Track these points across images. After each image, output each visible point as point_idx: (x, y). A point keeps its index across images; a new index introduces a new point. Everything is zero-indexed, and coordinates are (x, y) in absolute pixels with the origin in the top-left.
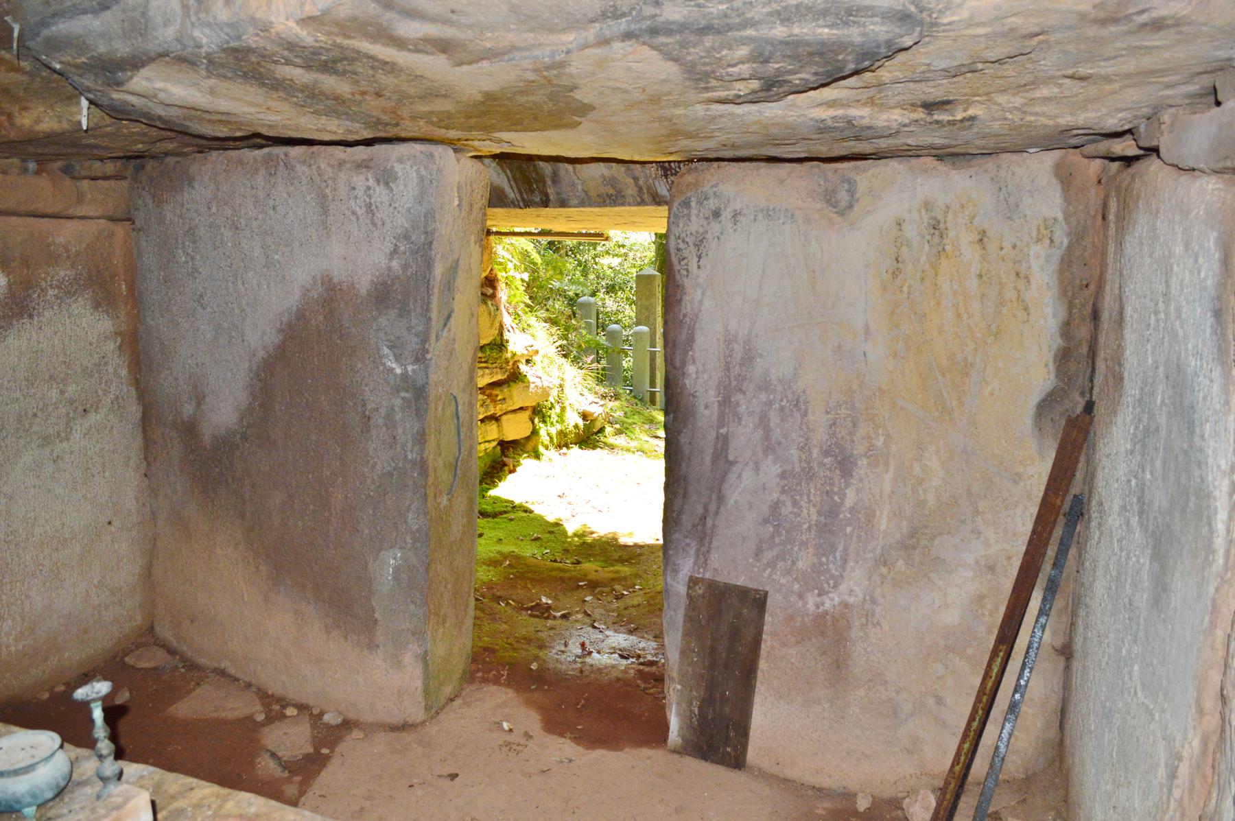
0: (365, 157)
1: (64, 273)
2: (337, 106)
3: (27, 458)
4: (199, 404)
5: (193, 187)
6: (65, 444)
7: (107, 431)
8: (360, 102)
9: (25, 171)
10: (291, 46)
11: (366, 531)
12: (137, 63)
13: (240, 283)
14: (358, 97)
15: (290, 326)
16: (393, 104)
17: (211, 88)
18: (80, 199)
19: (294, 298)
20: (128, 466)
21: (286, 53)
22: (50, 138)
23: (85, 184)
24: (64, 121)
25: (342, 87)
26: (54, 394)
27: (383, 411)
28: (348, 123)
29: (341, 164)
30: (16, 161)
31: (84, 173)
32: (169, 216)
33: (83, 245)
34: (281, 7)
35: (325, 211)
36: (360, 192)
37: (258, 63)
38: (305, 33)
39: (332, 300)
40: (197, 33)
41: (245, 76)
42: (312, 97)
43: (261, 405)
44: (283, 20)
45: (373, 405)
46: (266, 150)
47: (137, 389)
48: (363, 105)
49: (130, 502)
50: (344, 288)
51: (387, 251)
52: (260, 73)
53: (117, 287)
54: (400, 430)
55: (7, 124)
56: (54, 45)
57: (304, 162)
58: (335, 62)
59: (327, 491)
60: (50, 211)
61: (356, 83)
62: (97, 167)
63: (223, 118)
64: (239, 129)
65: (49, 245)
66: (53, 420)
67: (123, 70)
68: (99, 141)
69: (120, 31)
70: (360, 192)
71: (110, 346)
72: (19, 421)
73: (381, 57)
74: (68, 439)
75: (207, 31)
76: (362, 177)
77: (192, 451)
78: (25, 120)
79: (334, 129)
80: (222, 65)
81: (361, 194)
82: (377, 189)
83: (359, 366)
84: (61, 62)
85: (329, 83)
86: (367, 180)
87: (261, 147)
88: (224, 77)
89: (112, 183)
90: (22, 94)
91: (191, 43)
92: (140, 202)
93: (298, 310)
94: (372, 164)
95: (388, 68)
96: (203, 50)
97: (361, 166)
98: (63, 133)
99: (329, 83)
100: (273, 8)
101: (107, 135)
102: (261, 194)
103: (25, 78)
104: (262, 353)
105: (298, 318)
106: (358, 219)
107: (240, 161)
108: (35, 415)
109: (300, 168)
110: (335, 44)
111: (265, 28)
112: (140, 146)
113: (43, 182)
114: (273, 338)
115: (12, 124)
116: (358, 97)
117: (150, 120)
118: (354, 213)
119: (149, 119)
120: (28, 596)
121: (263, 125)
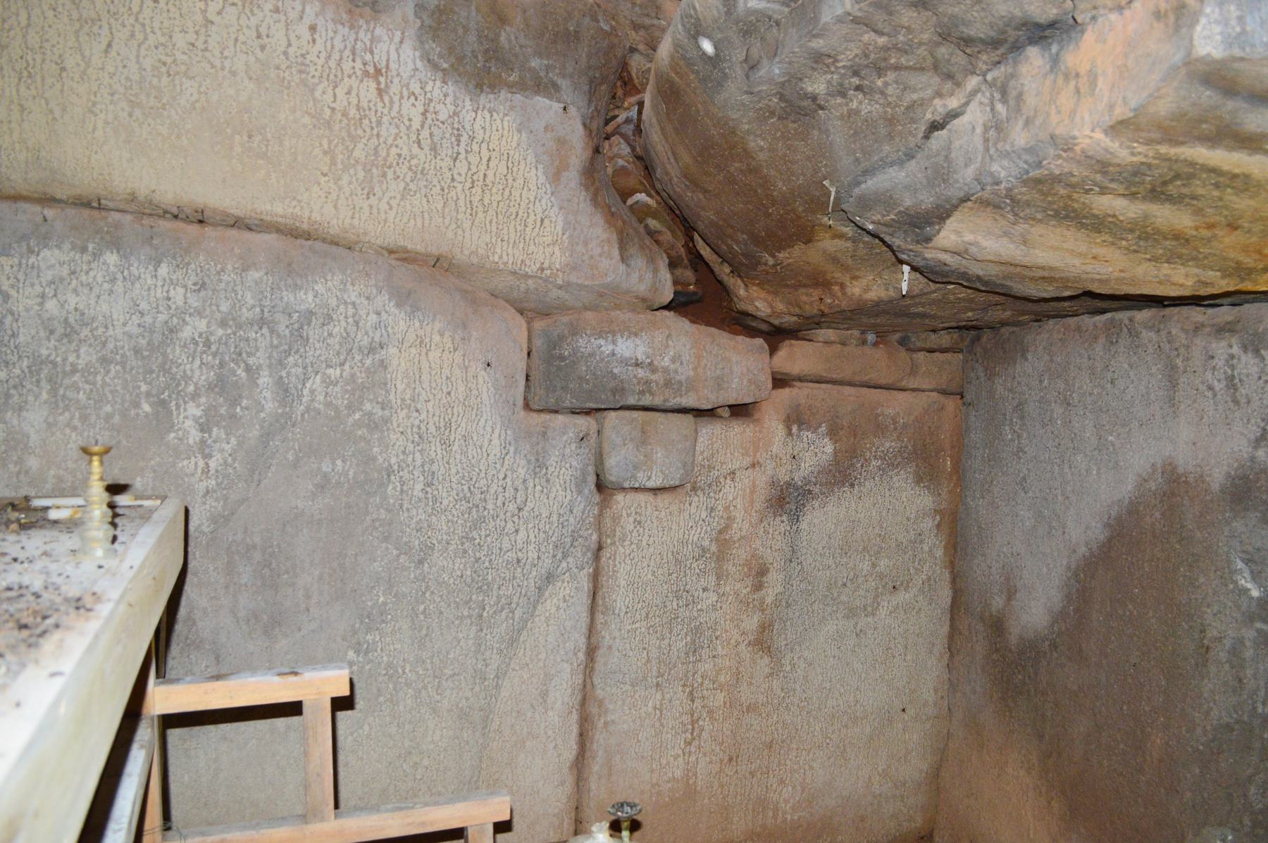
0: (1230, 318)
1: (889, 444)
2: (1179, 246)
3: (831, 627)
4: (1009, 599)
5: (1026, 359)
6: (870, 619)
7: (914, 613)
8: (1209, 241)
9: (864, 342)
10: (1103, 166)
11: (1189, 795)
12: (941, 214)
13: (1066, 466)
14: (1205, 233)
15: (1119, 519)
16: (1254, 239)
17: (1022, 235)
18: (914, 370)
19: (1127, 489)
20: (931, 652)
21: (1099, 177)
22: (879, 309)
23: (921, 356)
24: (891, 289)
25: (1182, 220)
26: (865, 566)
27: (1228, 643)
28: (1197, 271)
29: (1198, 328)
30: (856, 333)
31: (919, 344)
32: (1000, 390)
33: (912, 418)
34: (1087, 117)
35: (1173, 385)
36: (1220, 362)
37: (1069, 197)
38: (1117, 144)
39: (1173, 494)
40: (995, 167)
41: (1057, 215)
42: (1144, 236)
43: (1076, 610)
44: (1088, 133)
45: (1215, 633)
46: (1108, 315)
47: (952, 572)
48: (1214, 243)
49: (927, 694)
50: (1191, 479)
51: (1252, 437)
52: (1074, 211)
53: (941, 462)
54: (1249, 672)
55: (839, 294)
56: (866, 203)
57: (1151, 328)
58: (1165, 183)
59: (1143, 732)
60: (883, 381)
61: (1198, 212)
62: (933, 340)
63: (1046, 274)
64: (1067, 288)
65: (878, 415)
66: (862, 593)
67: (931, 224)
68: (927, 310)
69: (924, 181)
70: (1220, 362)
71: (928, 524)
72: (829, 589)
73: (1226, 168)
74: (873, 615)
75: (1005, 163)
76: (1223, 344)
77: (997, 650)
78: (855, 289)
79: (1182, 281)
80: (1028, 204)
81: (1221, 364)
82: (1243, 358)
83: (1202, 580)
84: (873, 222)
85: (1164, 215)
86: (1231, 347)
87: (1103, 312)
88: (1034, 219)
89: (949, 356)
90: (850, 262)
91: (989, 180)
92: (972, 375)
93: (1131, 502)
94: (1239, 326)
95: (1238, 183)
96: (1003, 186)
97: (1222, 330)
98: (891, 301)
99: (1164, 215)
100: (1078, 119)
101: (933, 302)
102: (1099, 366)
103: (849, 244)
104: (1084, 549)
105: (1130, 512)
106: (1215, 395)
107: (1079, 329)
108: (845, 585)
109: (1146, 335)
110: (1159, 156)
111: (1067, 146)
112: (970, 314)
113: (879, 354)
114: (1098, 533)
115: (844, 294)
116: (1205, 233)
117: (965, 280)
118: (1210, 388)
119: (968, 280)
120: (811, 768)
121: (1093, 280)
